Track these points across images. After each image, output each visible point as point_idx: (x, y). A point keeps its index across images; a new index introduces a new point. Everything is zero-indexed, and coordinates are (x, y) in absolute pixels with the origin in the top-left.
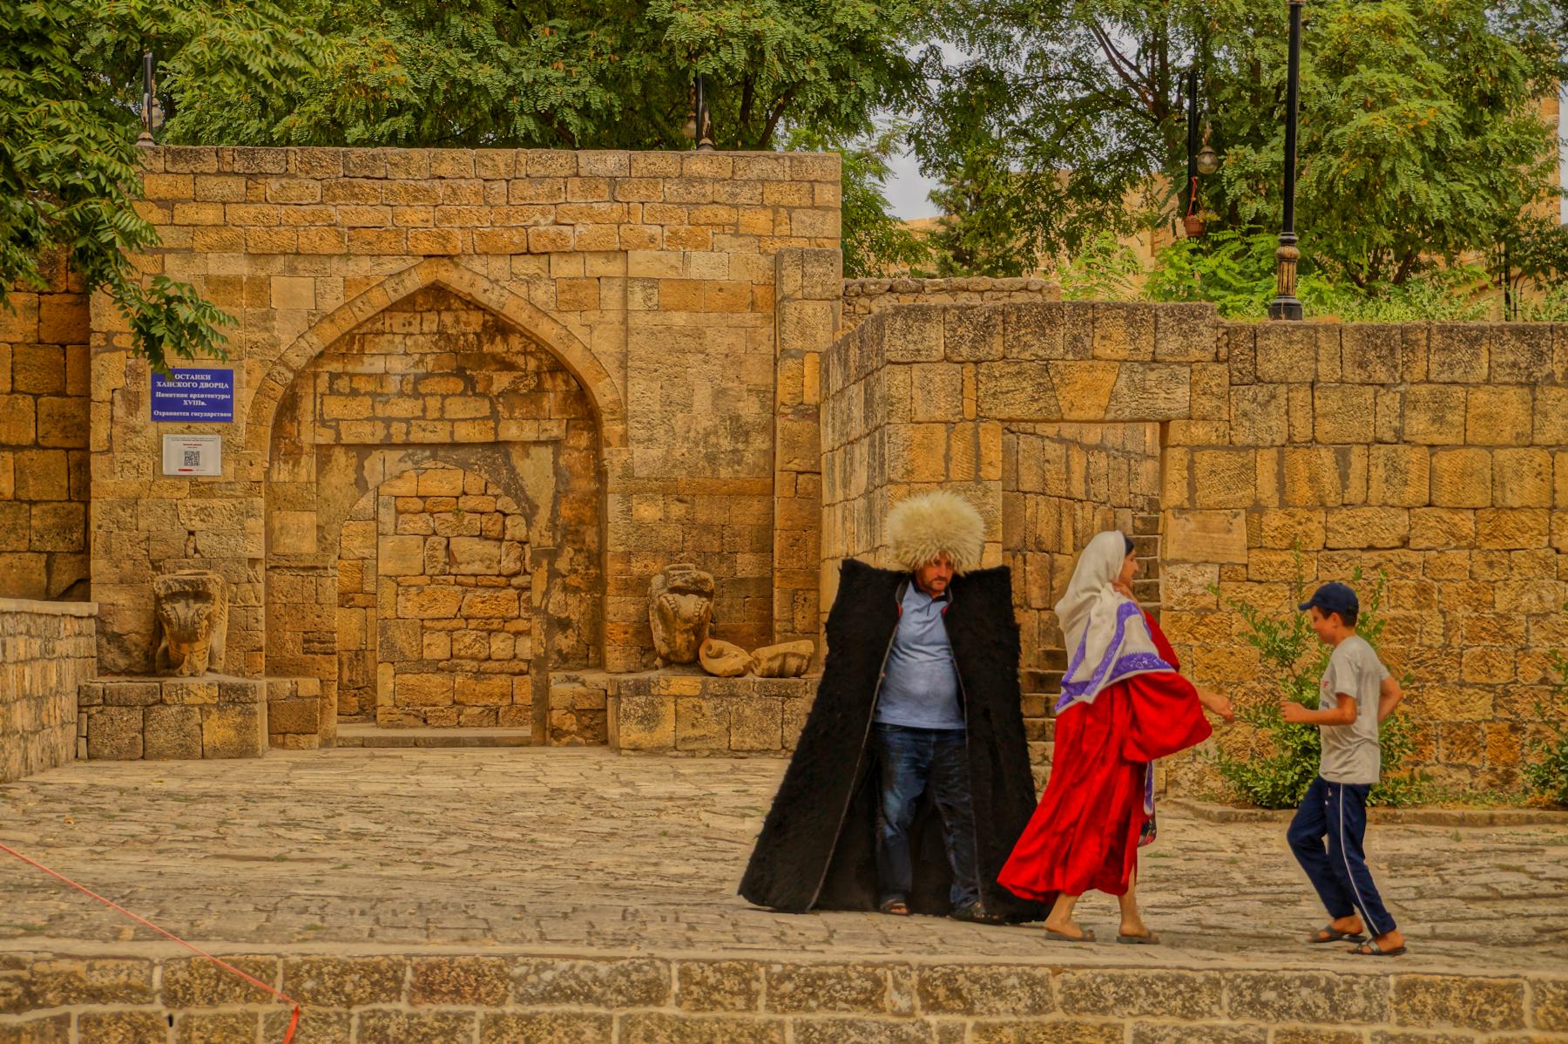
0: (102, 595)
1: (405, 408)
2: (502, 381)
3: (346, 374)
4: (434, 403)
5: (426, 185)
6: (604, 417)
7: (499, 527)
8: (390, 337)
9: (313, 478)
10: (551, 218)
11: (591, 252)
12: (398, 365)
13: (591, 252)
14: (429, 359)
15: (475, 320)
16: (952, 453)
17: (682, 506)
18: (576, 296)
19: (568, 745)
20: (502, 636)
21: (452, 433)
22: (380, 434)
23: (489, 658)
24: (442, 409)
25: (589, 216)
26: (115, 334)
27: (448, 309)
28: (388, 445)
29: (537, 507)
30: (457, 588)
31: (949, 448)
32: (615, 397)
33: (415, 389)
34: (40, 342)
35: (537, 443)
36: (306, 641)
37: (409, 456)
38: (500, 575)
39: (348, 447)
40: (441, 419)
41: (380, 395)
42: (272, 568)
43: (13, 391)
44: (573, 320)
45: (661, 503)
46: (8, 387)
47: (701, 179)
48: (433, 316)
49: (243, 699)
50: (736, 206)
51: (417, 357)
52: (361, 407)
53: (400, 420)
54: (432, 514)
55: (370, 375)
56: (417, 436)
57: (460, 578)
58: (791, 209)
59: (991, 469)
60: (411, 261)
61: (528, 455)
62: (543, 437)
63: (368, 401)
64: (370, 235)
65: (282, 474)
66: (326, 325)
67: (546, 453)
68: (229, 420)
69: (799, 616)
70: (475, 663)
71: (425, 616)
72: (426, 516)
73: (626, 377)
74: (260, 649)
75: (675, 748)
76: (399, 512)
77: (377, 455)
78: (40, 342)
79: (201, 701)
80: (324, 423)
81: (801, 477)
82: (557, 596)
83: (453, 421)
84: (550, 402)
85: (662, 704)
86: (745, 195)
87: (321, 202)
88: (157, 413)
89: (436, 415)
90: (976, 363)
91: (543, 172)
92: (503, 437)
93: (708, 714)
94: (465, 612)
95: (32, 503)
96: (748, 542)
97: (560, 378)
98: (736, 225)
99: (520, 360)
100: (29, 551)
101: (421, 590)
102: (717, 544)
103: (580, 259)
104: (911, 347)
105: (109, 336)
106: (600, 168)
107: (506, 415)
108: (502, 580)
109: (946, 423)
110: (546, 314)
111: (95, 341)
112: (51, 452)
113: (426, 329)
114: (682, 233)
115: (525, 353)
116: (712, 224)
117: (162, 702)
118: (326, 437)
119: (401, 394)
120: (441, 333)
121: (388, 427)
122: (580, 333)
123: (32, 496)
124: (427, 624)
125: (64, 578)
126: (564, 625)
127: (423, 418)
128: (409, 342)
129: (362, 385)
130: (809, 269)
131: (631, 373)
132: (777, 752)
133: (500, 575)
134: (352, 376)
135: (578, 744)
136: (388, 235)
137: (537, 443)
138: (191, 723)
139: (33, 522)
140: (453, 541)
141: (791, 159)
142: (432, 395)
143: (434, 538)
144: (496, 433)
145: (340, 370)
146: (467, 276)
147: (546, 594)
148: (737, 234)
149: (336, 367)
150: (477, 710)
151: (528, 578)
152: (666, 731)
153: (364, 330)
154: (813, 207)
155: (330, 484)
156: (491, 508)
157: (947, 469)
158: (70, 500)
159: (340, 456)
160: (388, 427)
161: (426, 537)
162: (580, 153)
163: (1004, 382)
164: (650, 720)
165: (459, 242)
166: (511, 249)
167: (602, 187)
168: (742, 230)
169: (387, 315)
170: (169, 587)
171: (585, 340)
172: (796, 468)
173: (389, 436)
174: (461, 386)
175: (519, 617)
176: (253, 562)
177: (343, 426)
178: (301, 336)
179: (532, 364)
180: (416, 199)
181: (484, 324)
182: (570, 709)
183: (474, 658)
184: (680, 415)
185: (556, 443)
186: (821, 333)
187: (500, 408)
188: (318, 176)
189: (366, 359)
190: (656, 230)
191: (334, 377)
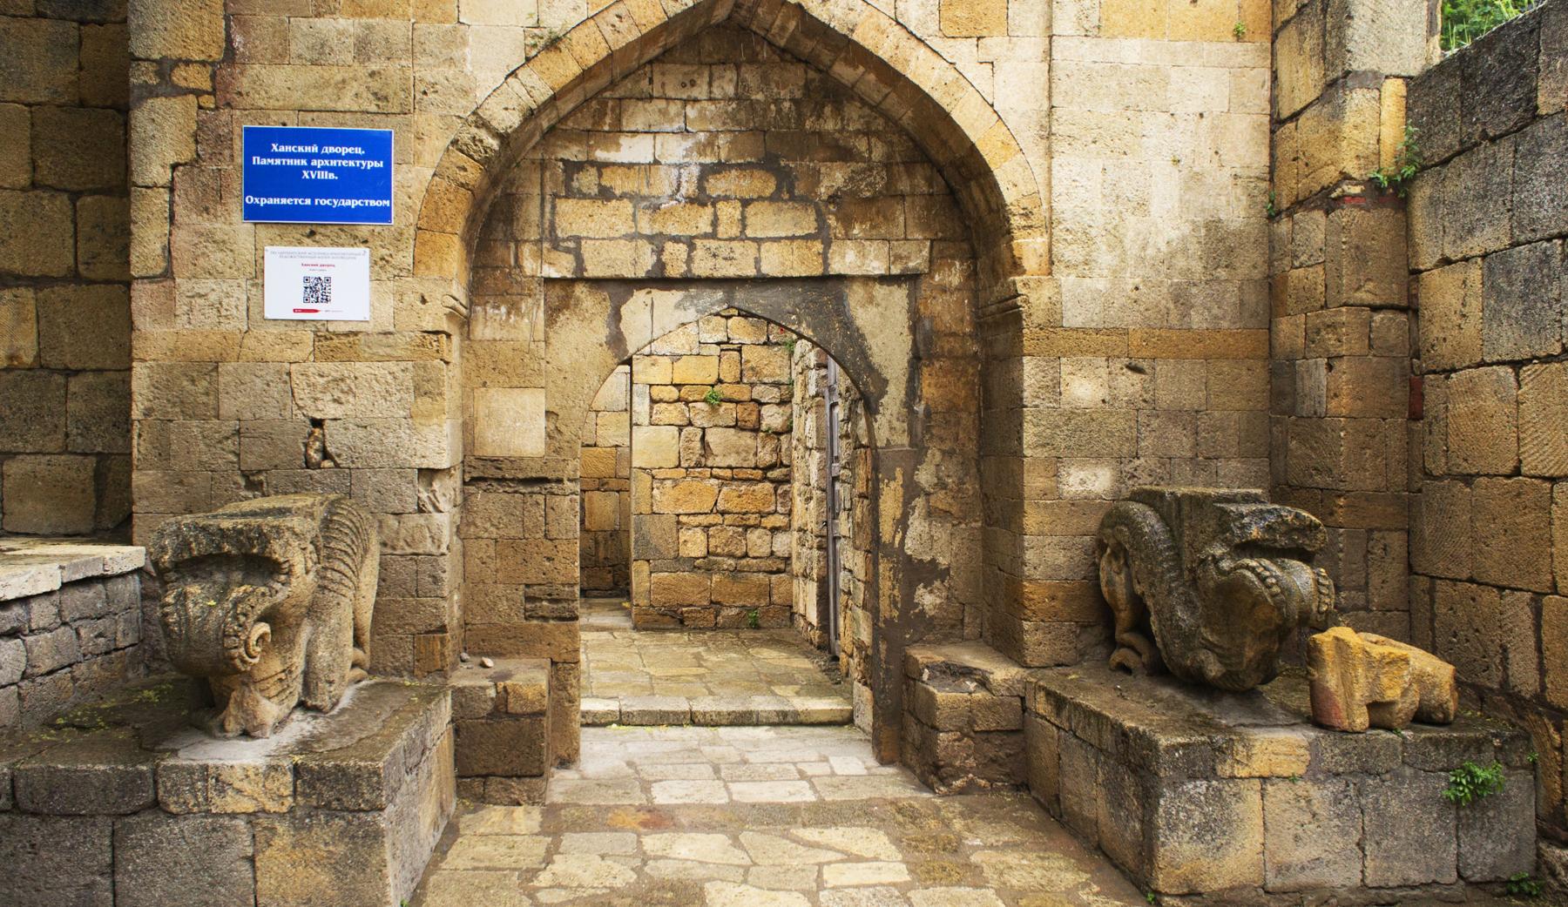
2: (835, 178)
6: (1016, 221)
7: (754, 417)
8: (662, 104)
12: (675, 149)
14: (722, 140)
17: (1136, 377)
21: (757, 261)
22: (646, 264)
23: (746, 555)
24: (743, 221)
26: (178, 62)
27: (753, 60)
28: (659, 280)
29: (886, 382)
30: (714, 481)
32: (1031, 188)
35: (885, 279)
36: (529, 599)
38: (756, 468)
39: (597, 283)
40: (742, 237)
41: (644, 198)
42: (474, 480)
43: (34, 185)
44: (963, 51)
45: (1103, 372)
46: (24, 179)
49: (349, 801)
51: (702, 136)
54: (687, 403)
55: (630, 166)
56: (702, 268)
57: (716, 471)
61: (871, 300)
62: (896, 270)
63: (627, 207)
67: (899, 295)
68: (383, 215)
70: (731, 561)
71: (681, 511)
72: (681, 405)
73: (1049, 153)
76: (653, 401)
77: (640, 297)
79: (249, 806)
80: (556, 244)
81: (1378, 317)
83: (758, 241)
85: (1237, 796)
88: (251, 200)
89: (735, 231)
92: (837, 267)
93: (1322, 813)
94: (720, 507)
95: (69, 373)
96: (1234, 441)
99: (861, 145)
100: (65, 451)
101: (676, 482)
102: (1187, 442)
105: (165, 67)
107: (840, 232)
111: (142, 76)
112: (101, 289)
113: (717, 93)
115: (867, 133)
118: (560, 267)
122: (974, 72)
123: (69, 360)
124: (683, 519)
127: (713, 236)
128: (691, 112)
133: (756, 468)
134: (601, 166)
137: (885, 279)
139: (71, 405)
142: (726, 199)
143: (690, 429)
144: (826, 263)
145: (582, 158)
147: (902, 524)
149: (573, 153)
150: (734, 612)
151: (784, 470)
153: (620, 93)
156: (746, 397)
161: (681, 428)
169: (657, 68)
171: (986, 89)
173: (661, 265)
174: (770, 188)
175: (776, 512)
176: (428, 474)
177: (587, 249)
178: (513, 74)
179: (878, 153)
181: (806, 86)
185: (909, 279)
187: (832, 221)
189: (624, 141)
191: (573, 168)
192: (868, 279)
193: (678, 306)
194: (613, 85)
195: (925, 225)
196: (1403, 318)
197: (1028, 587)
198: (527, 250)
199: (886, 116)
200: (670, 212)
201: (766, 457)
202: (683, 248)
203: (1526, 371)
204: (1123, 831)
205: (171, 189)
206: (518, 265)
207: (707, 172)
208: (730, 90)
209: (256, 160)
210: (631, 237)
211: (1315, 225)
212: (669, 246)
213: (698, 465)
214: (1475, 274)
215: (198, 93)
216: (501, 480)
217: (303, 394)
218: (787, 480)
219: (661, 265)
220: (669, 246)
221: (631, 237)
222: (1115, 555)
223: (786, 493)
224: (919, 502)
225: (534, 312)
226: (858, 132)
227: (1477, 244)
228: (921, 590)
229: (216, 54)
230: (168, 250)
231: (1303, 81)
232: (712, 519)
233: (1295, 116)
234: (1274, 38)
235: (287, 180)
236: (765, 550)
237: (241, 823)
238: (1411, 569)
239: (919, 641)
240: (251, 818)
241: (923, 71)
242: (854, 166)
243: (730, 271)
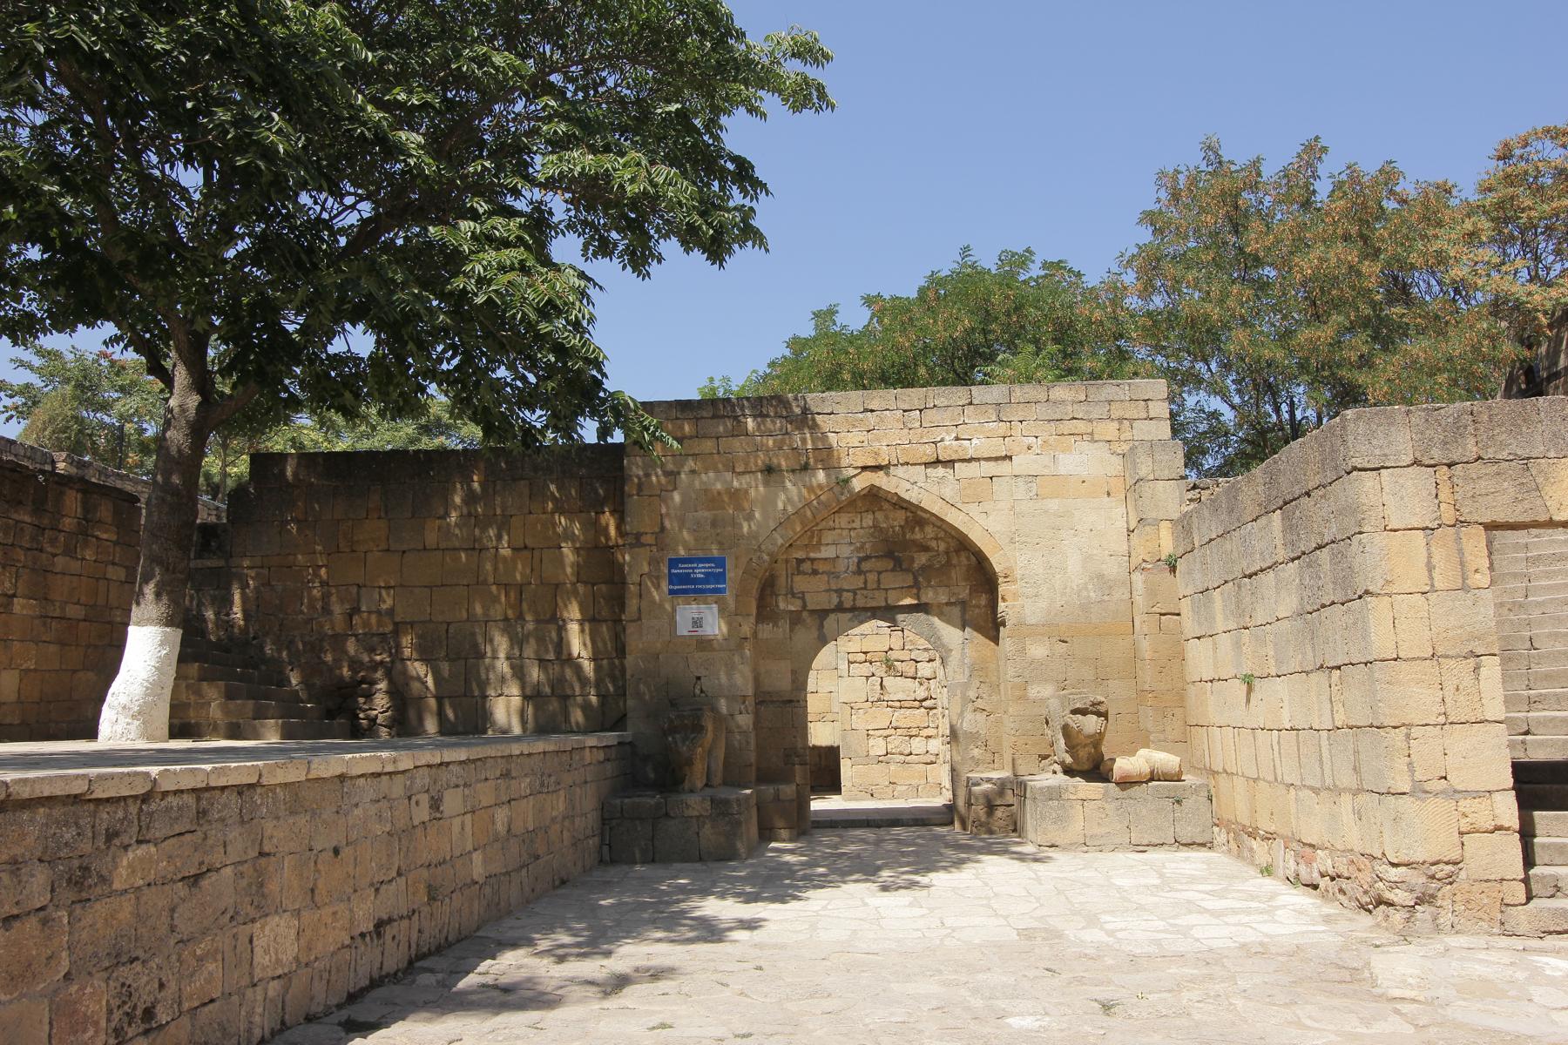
2: (921, 559)
3: (809, 559)
4: (872, 577)
5: (861, 416)
6: (1000, 580)
7: (913, 669)
10: (954, 435)
15: (899, 517)
16: (1434, 561)
20: (918, 739)
27: (881, 509)
31: (1430, 557)
39: (812, 612)
40: (878, 588)
44: (974, 510)
45: (1047, 643)
48: (870, 516)
50: (1090, 421)
52: (819, 583)
53: (848, 591)
56: (860, 603)
59: (1478, 576)
63: (825, 578)
65: (766, 631)
74: (751, 765)
76: (850, 662)
77: (832, 616)
79: (696, 813)
82: (969, 716)
83: (886, 590)
84: (956, 574)
86: (1096, 412)
89: (875, 586)
90: (1449, 466)
91: (946, 404)
94: (894, 724)
97: (963, 555)
98: (1092, 434)
99: (933, 544)
104: (1377, 452)
109: (1423, 529)
113: (864, 525)
118: (794, 606)
121: (840, 597)
127: (865, 588)
129: (821, 567)
130: (1157, 457)
134: (813, 560)
149: (800, 555)
157: (1431, 578)
160: (840, 597)
162: (972, 388)
163: (1483, 483)
168: (1096, 437)
172: (1159, 610)
173: (841, 603)
174: (891, 565)
177: (807, 597)
179: (942, 546)
184: (1058, 576)
187: (921, 579)
191: (800, 561)
194: (817, 524)
198: (780, 598)
200: (845, 578)
201: (921, 694)
202: (851, 594)
206: (777, 606)
207: (861, 560)
209: (673, 571)
210: (827, 591)
212: (845, 594)
213: (879, 700)
216: (772, 702)
219: (841, 603)
220: (845, 594)
221: (827, 591)
225: (784, 625)
229: (657, 530)
230: (639, 609)
235: (685, 579)
237: (694, 820)
240: (698, 817)
241: (954, 518)
243: (874, 604)
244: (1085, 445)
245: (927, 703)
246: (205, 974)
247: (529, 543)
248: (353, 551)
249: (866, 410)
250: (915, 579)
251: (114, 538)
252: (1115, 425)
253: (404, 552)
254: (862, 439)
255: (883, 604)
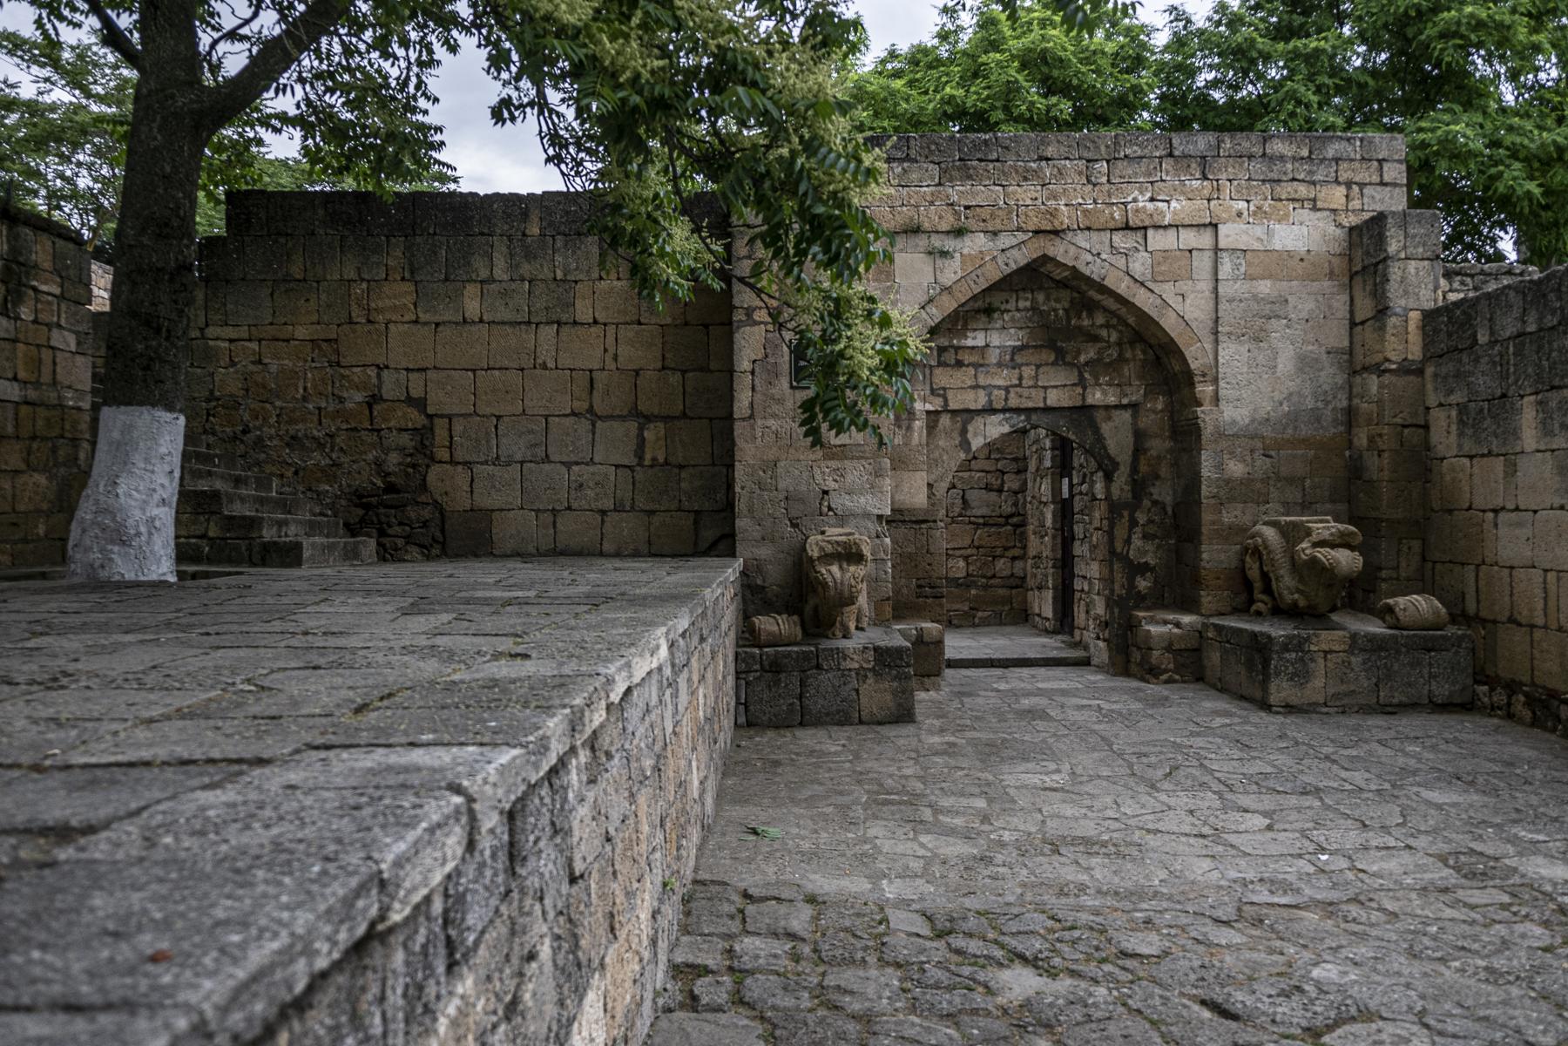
0: (747, 551)
1: (1002, 378)
6: (1197, 379)
9: (924, 440)
10: (1149, 195)
11: (1184, 226)
13: (1184, 226)
18: (1174, 266)
19: (1166, 682)
23: (994, 576)
25: (1183, 193)
27: (1041, 288)
33: (1012, 359)
34: (686, 324)
36: (919, 586)
37: (1006, 420)
39: (954, 412)
40: (1036, 386)
43: (664, 368)
46: (659, 365)
47: (1282, 158)
50: (1314, 183)
52: (965, 377)
55: (973, 348)
58: (1362, 185)
60: (1021, 237)
62: (1125, 401)
63: (972, 371)
64: (985, 213)
66: (945, 298)
67: (1126, 416)
69: (1403, 564)
73: (1217, 342)
75: (1325, 705)
77: (979, 421)
78: (686, 324)
79: (856, 666)
81: (1406, 431)
83: (1046, 388)
85: (1312, 660)
87: (940, 184)
89: (1031, 383)
91: (1139, 153)
92: (1090, 401)
95: (681, 467)
98: (1314, 200)
99: (1104, 333)
100: (679, 510)
102: (1299, 495)
103: (1172, 232)
105: (749, 312)
106: (1190, 150)
107: (1092, 381)
108: (1002, 520)
110: (1142, 284)
111: (738, 316)
114: (1266, 208)
115: (1107, 326)
116: (1293, 200)
117: (818, 667)
119: (1000, 365)
120: (1033, 309)
123: (680, 460)
125: (709, 535)
126: (1143, 569)
127: (1020, 385)
128: (1006, 317)
129: (967, 358)
130: (1411, 231)
131: (1221, 338)
132: (1423, 706)
134: (957, 349)
135: (1175, 681)
136: (1000, 213)
138: (847, 688)
140: (968, 493)
141: (1362, 140)
144: (1084, 399)
146: (1072, 250)
147: (1128, 541)
148: (1315, 209)
152: (1317, 686)
154: (1382, 184)
155: (937, 446)
158: (714, 464)
159: (945, 420)
164: (1301, 676)
165: (1065, 217)
166: (1112, 225)
167: (1194, 165)
168: (1320, 205)
170: (822, 549)
171: (1179, 308)
173: (990, 402)
174: (1052, 358)
177: (950, 395)
179: (1114, 337)
180: (1026, 179)
182: (1168, 648)
183: (984, 577)
185: (1134, 407)
186: (1423, 292)
187: (1087, 375)
188: (936, 159)
190: (1242, 205)
192: (1107, 407)
193: (1000, 423)
195: (1141, 377)
196: (1421, 431)
197: (1203, 573)
199: (1119, 318)
201: (1007, 509)
203: (1475, 461)
204: (1258, 694)
205: (753, 373)
208: (1028, 304)
211: (1373, 383)
214: (1454, 413)
215: (766, 324)
216: (904, 522)
217: (818, 477)
218: (1023, 524)
219: (990, 402)
220: (996, 392)
221: (972, 387)
222: (1253, 554)
223: (1023, 533)
224: (1138, 529)
226: (1101, 326)
227: (1454, 399)
228: (1138, 579)
231: (1365, 308)
232: (969, 551)
233: (1363, 323)
234: (1351, 279)
236: (1007, 573)
238: (1424, 559)
239: (1137, 607)
242: (1099, 345)
243: (1030, 405)
244: (1305, 214)
245: (1015, 520)
246: (456, 1002)
247: (601, 318)
248: (369, 321)
249: (1041, 158)
250: (1081, 375)
251: (57, 290)
252: (1342, 190)
253: (437, 325)
254: (1035, 195)
255: (1041, 405)
